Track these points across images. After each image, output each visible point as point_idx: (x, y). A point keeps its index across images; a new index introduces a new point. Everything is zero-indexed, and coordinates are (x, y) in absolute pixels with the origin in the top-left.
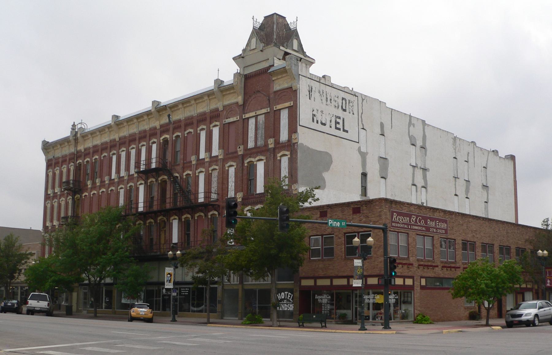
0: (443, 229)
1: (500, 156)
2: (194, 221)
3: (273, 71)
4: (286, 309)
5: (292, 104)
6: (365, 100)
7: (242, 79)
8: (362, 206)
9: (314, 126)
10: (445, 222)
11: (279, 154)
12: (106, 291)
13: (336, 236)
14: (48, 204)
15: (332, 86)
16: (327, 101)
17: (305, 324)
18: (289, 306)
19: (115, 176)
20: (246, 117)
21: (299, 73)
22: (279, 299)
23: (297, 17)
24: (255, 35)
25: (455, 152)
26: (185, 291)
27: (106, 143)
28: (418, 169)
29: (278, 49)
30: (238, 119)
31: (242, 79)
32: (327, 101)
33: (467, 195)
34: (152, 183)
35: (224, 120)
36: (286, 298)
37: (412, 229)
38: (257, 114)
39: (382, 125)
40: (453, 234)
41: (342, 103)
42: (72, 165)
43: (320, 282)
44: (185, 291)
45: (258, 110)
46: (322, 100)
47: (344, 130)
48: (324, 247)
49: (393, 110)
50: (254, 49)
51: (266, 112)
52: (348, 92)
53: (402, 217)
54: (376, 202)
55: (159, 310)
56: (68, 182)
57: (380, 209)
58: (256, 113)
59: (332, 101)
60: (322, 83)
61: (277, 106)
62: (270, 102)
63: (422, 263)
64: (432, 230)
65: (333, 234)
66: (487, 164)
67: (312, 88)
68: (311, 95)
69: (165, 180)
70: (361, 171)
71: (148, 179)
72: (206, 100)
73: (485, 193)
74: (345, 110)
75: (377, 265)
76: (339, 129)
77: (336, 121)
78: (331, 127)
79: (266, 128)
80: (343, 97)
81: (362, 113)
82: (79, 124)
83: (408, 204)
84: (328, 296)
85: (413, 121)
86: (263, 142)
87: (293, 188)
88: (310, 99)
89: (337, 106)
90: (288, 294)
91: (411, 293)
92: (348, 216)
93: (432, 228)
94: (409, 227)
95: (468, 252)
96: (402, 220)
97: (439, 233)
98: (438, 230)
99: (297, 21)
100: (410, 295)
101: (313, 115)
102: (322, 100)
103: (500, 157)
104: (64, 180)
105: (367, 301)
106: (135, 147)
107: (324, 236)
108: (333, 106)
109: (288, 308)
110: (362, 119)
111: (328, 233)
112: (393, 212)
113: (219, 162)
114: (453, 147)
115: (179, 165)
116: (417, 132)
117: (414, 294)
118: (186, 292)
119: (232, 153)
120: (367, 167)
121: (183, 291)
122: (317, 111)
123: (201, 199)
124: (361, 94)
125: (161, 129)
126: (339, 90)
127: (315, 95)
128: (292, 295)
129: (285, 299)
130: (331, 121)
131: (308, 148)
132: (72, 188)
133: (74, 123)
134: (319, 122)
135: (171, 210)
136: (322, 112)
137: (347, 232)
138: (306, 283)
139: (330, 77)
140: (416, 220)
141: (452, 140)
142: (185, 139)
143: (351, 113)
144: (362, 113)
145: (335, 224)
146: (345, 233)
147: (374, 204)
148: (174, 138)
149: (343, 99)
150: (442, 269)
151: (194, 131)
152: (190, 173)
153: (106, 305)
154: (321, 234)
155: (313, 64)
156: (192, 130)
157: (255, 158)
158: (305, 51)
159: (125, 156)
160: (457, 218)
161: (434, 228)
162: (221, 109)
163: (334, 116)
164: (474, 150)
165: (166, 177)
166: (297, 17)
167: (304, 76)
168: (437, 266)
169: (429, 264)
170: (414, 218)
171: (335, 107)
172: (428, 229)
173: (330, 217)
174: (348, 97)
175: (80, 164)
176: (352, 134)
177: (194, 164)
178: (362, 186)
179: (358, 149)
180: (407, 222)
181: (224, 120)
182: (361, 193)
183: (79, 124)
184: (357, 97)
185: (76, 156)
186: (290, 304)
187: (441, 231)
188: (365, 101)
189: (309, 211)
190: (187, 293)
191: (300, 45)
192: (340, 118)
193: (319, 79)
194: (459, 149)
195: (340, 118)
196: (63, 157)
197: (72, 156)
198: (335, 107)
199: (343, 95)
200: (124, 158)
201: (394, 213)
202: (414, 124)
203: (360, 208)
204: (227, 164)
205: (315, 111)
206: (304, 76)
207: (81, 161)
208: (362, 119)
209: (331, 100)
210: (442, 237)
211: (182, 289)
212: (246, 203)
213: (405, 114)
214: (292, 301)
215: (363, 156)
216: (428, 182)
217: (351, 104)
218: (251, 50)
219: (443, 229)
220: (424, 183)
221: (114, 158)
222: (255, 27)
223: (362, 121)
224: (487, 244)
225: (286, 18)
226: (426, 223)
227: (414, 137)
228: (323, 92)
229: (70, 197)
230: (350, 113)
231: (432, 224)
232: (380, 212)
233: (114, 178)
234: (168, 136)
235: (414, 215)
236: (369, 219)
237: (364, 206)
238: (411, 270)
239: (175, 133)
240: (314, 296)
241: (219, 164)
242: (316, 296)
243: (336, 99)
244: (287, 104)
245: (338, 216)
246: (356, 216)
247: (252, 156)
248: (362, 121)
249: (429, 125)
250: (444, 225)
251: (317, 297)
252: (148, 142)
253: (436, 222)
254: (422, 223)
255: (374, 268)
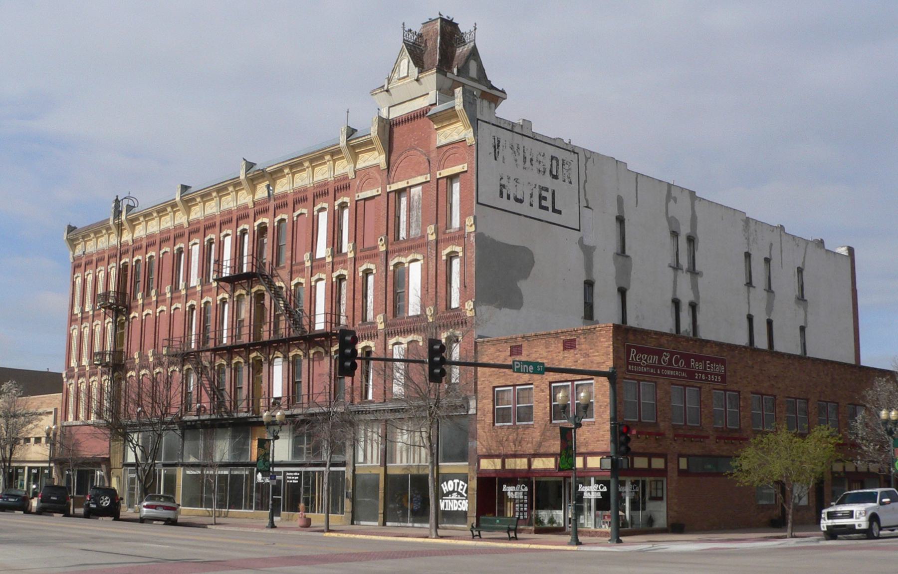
0: (718, 375)
1: (827, 248)
2: (230, 370)
3: (435, 114)
4: (456, 509)
5: (466, 169)
6: (591, 159)
7: (385, 126)
8: (578, 337)
9: (503, 203)
10: (722, 362)
11: (445, 251)
12: (165, 475)
13: (537, 387)
14: (86, 329)
15: (534, 137)
16: (525, 162)
17: (519, 536)
18: (461, 503)
19: (328, 251)
20: (392, 189)
21: (478, 117)
22: (445, 492)
23: (475, 24)
24: (406, 53)
25: (748, 244)
26: (293, 478)
27: (168, 230)
28: (683, 272)
29: (444, 77)
30: (379, 193)
31: (385, 126)
32: (525, 162)
33: (770, 316)
34: (400, 267)
35: (357, 195)
36: (456, 490)
37: (664, 375)
38: (409, 185)
39: (620, 200)
40: (736, 383)
41: (551, 165)
42: (113, 267)
43: (511, 464)
44: (293, 478)
45: (411, 177)
46: (516, 161)
47: (555, 211)
48: (553, 403)
49: (639, 175)
50: (404, 78)
51: (424, 180)
52: (562, 147)
53: (646, 356)
54: (600, 331)
55: (251, 508)
56: (106, 295)
57: (607, 342)
58: (408, 183)
59: (534, 162)
60: (516, 133)
61: (442, 171)
62: (431, 165)
63: (681, 432)
64: (698, 377)
65: (532, 384)
66: (804, 263)
67: (499, 141)
68: (498, 152)
69: (262, 292)
70: (584, 278)
71: (234, 291)
72: (328, 161)
73: (802, 312)
74: (555, 177)
75: (603, 435)
76: (546, 209)
77: (540, 195)
78: (531, 205)
79: (425, 208)
80: (553, 155)
81: (586, 181)
82: (125, 198)
83: (656, 333)
84: (523, 487)
85: (674, 193)
86: (419, 231)
87: (466, 307)
88: (496, 159)
89: (542, 169)
90: (458, 484)
91: (662, 481)
92: (556, 353)
93: (698, 373)
94: (659, 372)
95: (763, 413)
96: (645, 360)
97: (711, 381)
98: (709, 376)
99: (475, 29)
100: (660, 486)
101: (501, 185)
102: (516, 161)
103: (827, 250)
104: (100, 290)
105: (586, 496)
106: (230, 233)
107: (517, 387)
108: (536, 171)
109: (459, 507)
110: (585, 191)
111: (524, 383)
112: (629, 348)
113: (349, 263)
114: (744, 235)
115: (284, 267)
116: (681, 211)
117: (667, 484)
118: (294, 479)
119: (369, 249)
120: (594, 270)
121: (290, 478)
122: (509, 178)
123: (320, 325)
124: (584, 149)
125: (190, 228)
126: (546, 143)
127: (505, 152)
128: (466, 485)
129: (453, 491)
130: (531, 196)
131: (493, 241)
132: (112, 304)
133: (117, 196)
134: (512, 197)
135: (250, 345)
136: (516, 180)
137: (554, 380)
138: (485, 464)
139: (530, 122)
140: (671, 360)
141: (743, 223)
142: (160, 261)
143: (567, 180)
144: (586, 181)
145: (526, 368)
146: (551, 383)
147: (598, 334)
148: (336, 208)
149: (552, 158)
150: (717, 442)
151: (308, 211)
152: (302, 281)
153: (144, 500)
154: (512, 384)
155: (504, 101)
156: (305, 211)
157: (406, 256)
158: (489, 79)
159: (197, 253)
160: (742, 356)
161: (702, 373)
162: (351, 175)
163: (537, 186)
164: (781, 240)
165: (263, 288)
166: (475, 24)
167: (486, 122)
168: (707, 437)
169: (694, 433)
170: (666, 357)
171: (540, 171)
172: (691, 375)
173: (527, 356)
174: (561, 155)
175: (125, 266)
176: (569, 217)
177: (308, 267)
178: (585, 303)
179: (579, 241)
180: (655, 363)
181: (357, 195)
182: (583, 315)
183: (125, 198)
184: (576, 155)
185: (119, 251)
186: (462, 500)
187: (715, 378)
188: (590, 161)
189: (494, 345)
190: (296, 480)
191: (481, 70)
192: (547, 190)
193: (511, 126)
194: (754, 239)
195: (547, 190)
196: (98, 253)
197: (114, 252)
198: (540, 171)
199: (552, 151)
200: (197, 257)
201: (632, 350)
202: (675, 197)
203: (575, 340)
204: (444, 250)
205: (505, 179)
206: (486, 122)
207: (127, 260)
208: (585, 191)
209: (531, 160)
210: (716, 387)
211: (288, 474)
212: (391, 332)
213: (660, 181)
214: (465, 495)
215: (588, 251)
216: (700, 294)
217: (566, 167)
218: (400, 79)
219: (718, 375)
220: (693, 295)
221: (323, 220)
222: (407, 41)
223: (585, 195)
224: (796, 399)
225: (459, 26)
226: (688, 364)
227: (677, 221)
228: (518, 148)
229: (109, 319)
230: (564, 181)
231: (699, 366)
232: (607, 347)
233: (346, 251)
234: (266, 220)
235: (667, 352)
236: (590, 358)
237: (581, 337)
238: (661, 443)
239: (259, 219)
240: (577, 487)
241: (349, 267)
242: (580, 487)
243: (541, 158)
244: (421, 179)
245: (540, 354)
246: (570, 354)
247: (402, 254)
248: (585, 195)
249: (701, 199)
250: (720, 368)
251: (581, 488)
252: (234, 229)
253: (705, 363)
254: (681, 364)
255: (599, 441)
